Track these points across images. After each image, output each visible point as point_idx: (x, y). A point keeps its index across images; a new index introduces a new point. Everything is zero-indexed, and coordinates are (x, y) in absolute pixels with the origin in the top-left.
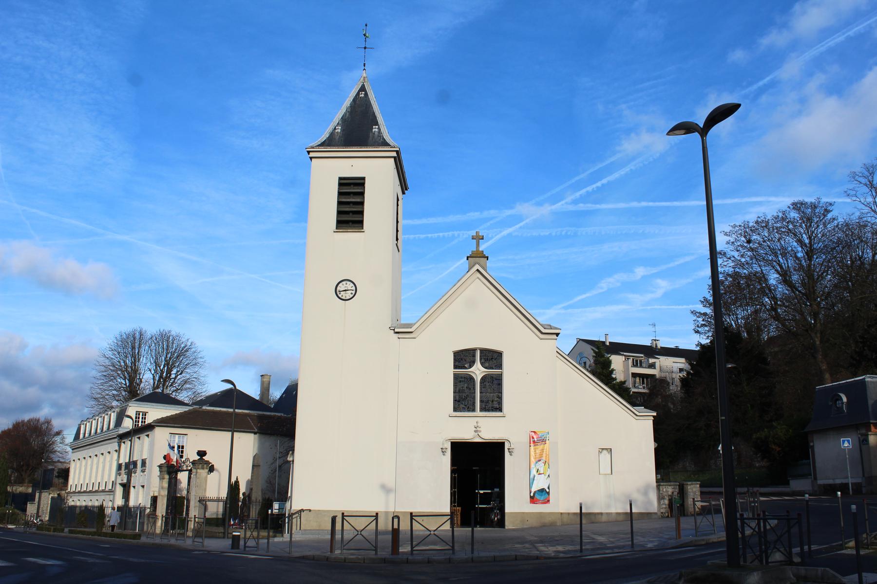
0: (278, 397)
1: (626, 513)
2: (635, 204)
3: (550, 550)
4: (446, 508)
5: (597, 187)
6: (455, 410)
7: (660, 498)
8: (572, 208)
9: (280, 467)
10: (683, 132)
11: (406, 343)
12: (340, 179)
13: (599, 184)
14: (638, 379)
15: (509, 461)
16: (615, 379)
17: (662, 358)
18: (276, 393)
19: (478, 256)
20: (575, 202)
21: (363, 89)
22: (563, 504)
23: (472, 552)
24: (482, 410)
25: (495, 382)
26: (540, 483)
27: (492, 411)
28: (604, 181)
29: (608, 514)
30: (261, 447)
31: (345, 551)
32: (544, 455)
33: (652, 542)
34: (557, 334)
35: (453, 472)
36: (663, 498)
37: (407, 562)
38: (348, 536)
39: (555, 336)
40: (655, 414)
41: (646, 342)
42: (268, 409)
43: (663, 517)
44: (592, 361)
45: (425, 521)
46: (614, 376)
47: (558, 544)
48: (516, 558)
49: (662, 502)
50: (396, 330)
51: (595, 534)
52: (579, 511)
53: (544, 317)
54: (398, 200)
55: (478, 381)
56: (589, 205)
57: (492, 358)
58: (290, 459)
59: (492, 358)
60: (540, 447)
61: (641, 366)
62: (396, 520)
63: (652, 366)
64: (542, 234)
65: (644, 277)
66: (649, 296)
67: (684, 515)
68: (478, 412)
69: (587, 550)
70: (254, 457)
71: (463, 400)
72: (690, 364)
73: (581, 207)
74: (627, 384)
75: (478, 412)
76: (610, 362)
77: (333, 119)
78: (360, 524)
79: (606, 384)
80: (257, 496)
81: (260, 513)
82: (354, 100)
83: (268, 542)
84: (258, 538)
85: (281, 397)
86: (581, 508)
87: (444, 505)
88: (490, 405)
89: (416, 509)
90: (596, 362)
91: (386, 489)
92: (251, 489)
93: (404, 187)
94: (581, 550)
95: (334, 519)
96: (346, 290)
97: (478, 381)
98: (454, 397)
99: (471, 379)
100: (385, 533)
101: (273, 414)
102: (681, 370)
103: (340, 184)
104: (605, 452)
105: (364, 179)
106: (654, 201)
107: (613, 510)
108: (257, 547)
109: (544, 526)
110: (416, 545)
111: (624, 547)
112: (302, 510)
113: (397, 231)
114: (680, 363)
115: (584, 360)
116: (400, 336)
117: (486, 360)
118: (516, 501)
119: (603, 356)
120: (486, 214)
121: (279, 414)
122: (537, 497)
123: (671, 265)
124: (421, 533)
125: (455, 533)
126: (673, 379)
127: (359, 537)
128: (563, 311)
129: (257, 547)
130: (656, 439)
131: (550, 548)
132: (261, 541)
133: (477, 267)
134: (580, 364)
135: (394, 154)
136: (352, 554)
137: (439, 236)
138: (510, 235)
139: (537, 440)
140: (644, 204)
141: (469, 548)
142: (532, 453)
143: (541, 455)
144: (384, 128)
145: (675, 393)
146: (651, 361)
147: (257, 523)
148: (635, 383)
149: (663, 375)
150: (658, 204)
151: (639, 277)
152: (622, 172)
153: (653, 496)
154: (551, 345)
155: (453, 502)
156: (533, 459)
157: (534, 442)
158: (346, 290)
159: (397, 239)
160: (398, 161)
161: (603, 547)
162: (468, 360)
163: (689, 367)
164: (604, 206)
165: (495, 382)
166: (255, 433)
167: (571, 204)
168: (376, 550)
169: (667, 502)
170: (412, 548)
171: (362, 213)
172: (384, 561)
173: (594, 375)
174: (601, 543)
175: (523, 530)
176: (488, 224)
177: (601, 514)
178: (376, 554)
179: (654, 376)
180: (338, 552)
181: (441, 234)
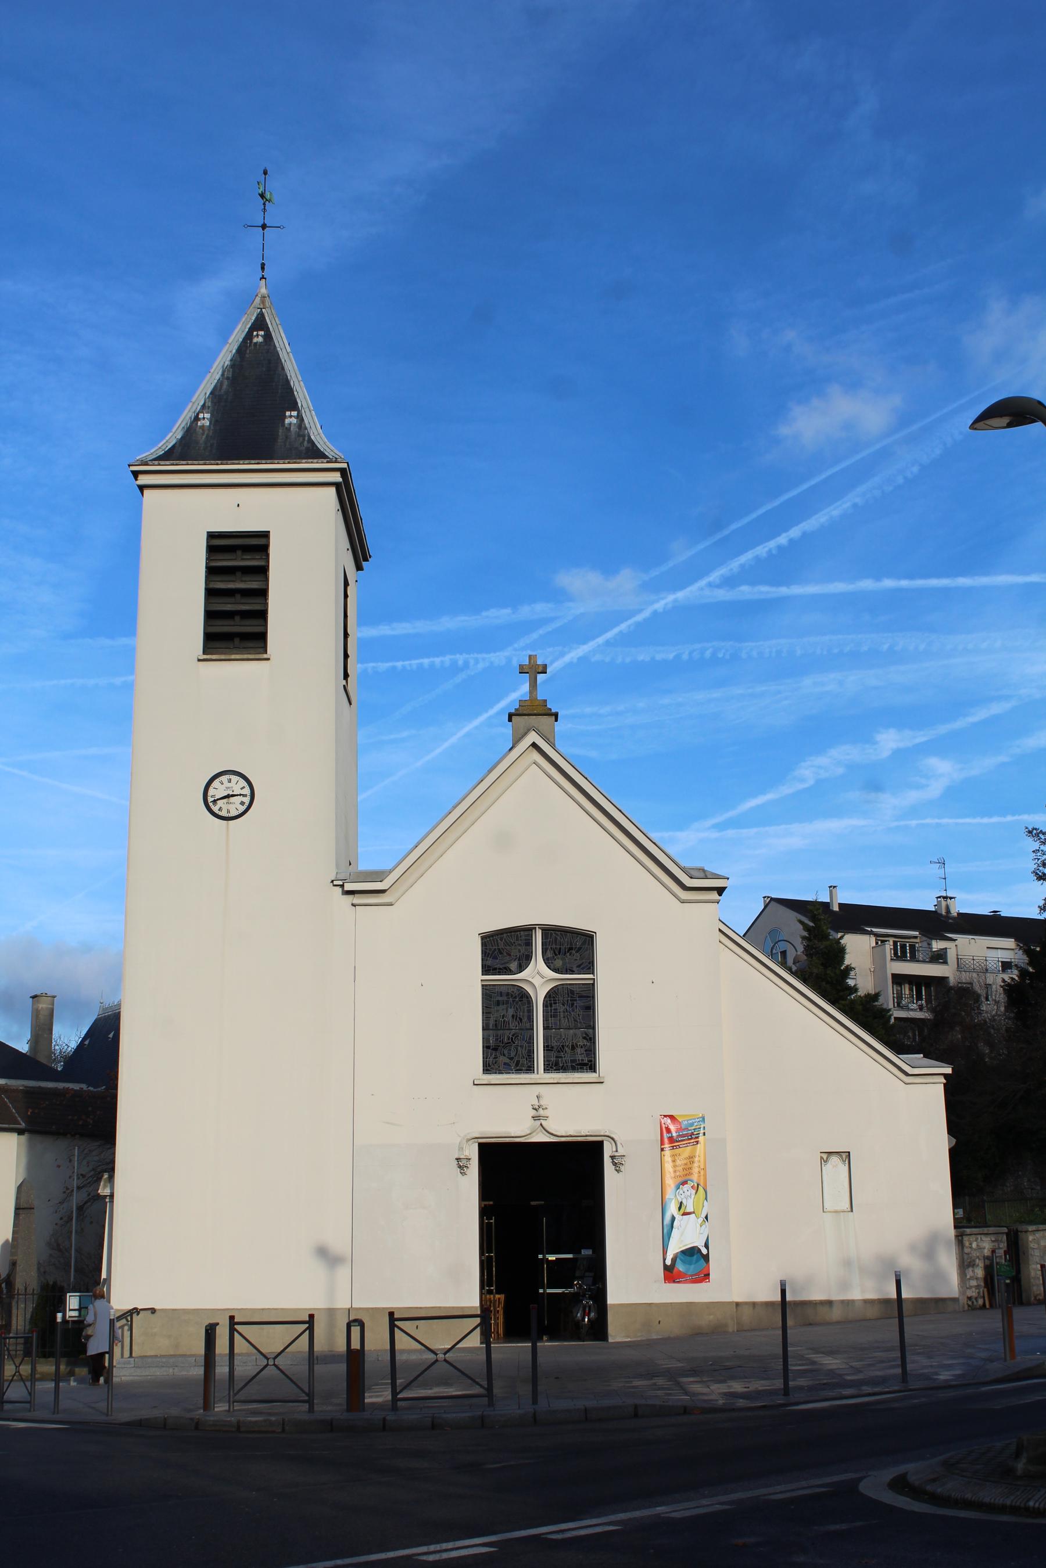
0: (73, 1045)
1: (885, 1302)
2: (867, 584)
3: (714, 1392)
4: (470, 1297)
5: (780, 548)
6: (487, 1069)
7: (965, 1264)
8: (723, 595)
9: (80, 1209)
10: (1006, 420)
11: (371, 916)
12: (211, 536)
13: (783, 540)
14: (906, 990)
15: (614, 1185)
16: (854, 989)
17: (962, 940)
18: (68, 1037)
19: (533, 712)
20: (729, 582)
21: (260, 323)
22: (741, 1280)
23: (535, 1401)
25: (579, 1003)
26: (687, 1235)
28: (795, 532)
29: (847, 1303)
30: (34, 1164)
31: (237, 1406)
32: (695, 1170)
33: (949, 1367)
34: (720, 891)
35: (484, 1212)
36: (972, 1264)
37: (385, 1426)
38: (245, 1368)
39: (714, 895)
40: (948, 1070)
41: (925, 901)
42: (47, 1073)
43: (972, 1308)
44: (801, 949)
45: (424, 1331)
46: (851, 982)
47: (733, 1378)
48: (636, 1412)
49: (969, 1273)
50: (348, 887)
51: (816, 1350)
52: (778, 1298)
53: (684, 845)
54: (346, 584)
55: (539, 1001)
56: (764, 589)
57: (572, 947)
58: (104, 1191)
59: (572, 947)
60: (686, 1151)
61: (914, 959)
62: (356, 1331)
63: (939, 957)
64: (659, 657)
65: (897, 753)
66: (913, 796)
67: (1021, 1303)
68: (540, 1074)
69: (801, 1388)
70: (19, 1189)
71: (505, 1048)
72: (1028, 952)
73: (745, 592)
74: (881, 1000)
75: (540, 1074)
76: (841, 951)
77: (192, 399)
78: (272, 1340)
79: (833, 1002)
80: (27, 1279)
81: (34, 1321)
82: (241, 351)
83: (57, 1387)
84: (33, 1378)
85: (81, 1046)
86: (783, 1292)
87: (469, 1295)
88: (567, 1057)
89: (403, 1300)
90: (809, 950)
91: (326, 1255)
92: (14, 1264)
93: (360, 553)
94: (786, 1391)
95: (210, 1332)
96: (228, 796)
97: (539, 1001)
98: (485, 1039)
99: (521, 998)
100: (331, 1358)
101: (61, 1085)
102: (1006, 966)
103: (211, 550)
104: (834, 1159)
105: (266, 535)
106: (911, 576)
107: (856, 1294)
108: (30, 1401)
109: (697, 1334)
110: (406, 1387)
111: (883, 1380)
112: (136, 1311)
113: (346, 656)
114: (1003, 949)
115: (782, 946)
116: (357, 899)
117: (557, 952)
118: (632, 1279)
119: (825, 937)
120: (526, 612)
121: (76, 1086)
122: (680, 1267)
123: (959, 724)
124: (413, 1357)
125: (494, 1356)
126: (988, 986)
127: (271, 1371)
128: (714, 835)
129: (30, 1401)
130: (953, 1128)
131: (714, 1387)
132: (40, 1386)
133: (533, 737)
134: (772, 956)
135: (337, 477)
136: (254, 1413)
138: (583, 660)
139: (678, 1135)
140: (888, 583)
141: (525, 1390)
142: (668, 1167)
143: (688, 1170)
144: (311, 415)
145: (993, 1019)
146: (937, 945)
147: (27, 1341)
148: (900, 997)
149: (965, 977)
150: (920, 583)
151: (886, 754)
152: (835, 511)
153: (948, 1262)
154: (704, 915)
155: (486, 1282)
156: (670, 1182)
157: (671, 1140)
158: (228, 796)
159: (346, 676)
160: (345, 492)
161: (836, 1382)
162: (515, 952)
163: (1025, 959)
164: (796, 590)
165: (579, 1003)
166: (20, 1132)
167: (718, 586)
168: (310, 1402)
169: (980, 1272)
170: (394, 1393)
172: (330, 1426)
173: (805, 981)
174: (831, 1373)
175: (649, 1344)
176: (535, 636)
177: (829, 1303)
178: (311, 1410)
179: (942, 980)
180: (220, 1407)
181: (426, 661)
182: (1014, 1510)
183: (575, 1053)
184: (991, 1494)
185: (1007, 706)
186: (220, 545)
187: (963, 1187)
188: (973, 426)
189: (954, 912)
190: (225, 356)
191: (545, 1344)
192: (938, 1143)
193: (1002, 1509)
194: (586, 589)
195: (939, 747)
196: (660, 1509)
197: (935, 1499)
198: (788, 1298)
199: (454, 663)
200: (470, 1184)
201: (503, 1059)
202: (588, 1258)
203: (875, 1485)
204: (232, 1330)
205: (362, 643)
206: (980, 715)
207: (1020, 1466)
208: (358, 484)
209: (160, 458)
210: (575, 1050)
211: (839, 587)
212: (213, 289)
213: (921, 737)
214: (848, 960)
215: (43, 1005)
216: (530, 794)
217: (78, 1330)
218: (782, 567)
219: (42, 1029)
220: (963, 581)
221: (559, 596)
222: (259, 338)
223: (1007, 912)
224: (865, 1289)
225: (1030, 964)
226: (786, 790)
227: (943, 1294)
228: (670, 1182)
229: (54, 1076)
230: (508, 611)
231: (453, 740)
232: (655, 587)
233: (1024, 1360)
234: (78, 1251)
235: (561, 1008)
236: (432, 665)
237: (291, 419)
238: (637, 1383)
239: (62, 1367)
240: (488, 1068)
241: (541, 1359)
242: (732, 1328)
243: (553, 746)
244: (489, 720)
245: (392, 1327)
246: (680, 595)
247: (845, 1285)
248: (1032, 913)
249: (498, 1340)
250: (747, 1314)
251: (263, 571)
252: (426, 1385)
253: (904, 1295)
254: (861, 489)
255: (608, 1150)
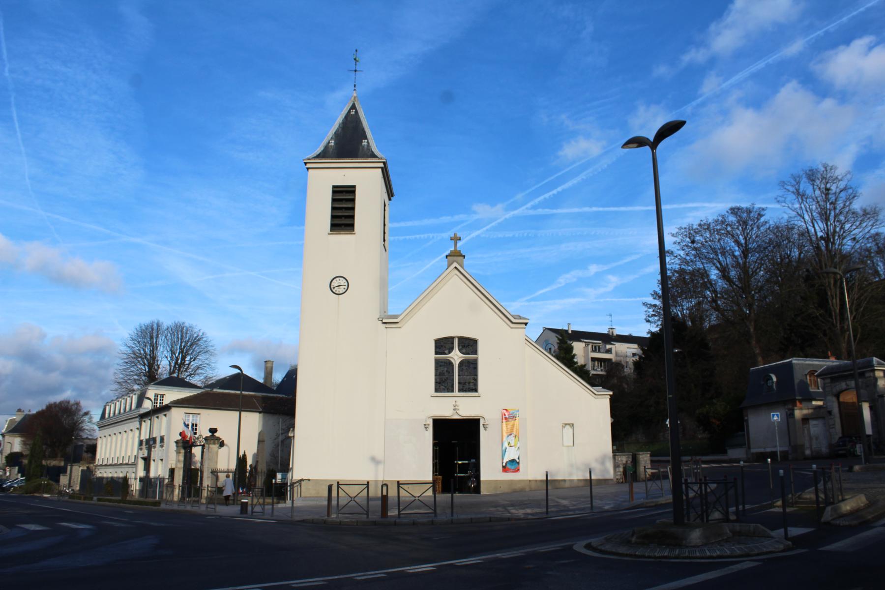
0: (280, 380)
1: (586, 480)
2: (587, 209)
3: (520, 513)
4: (430, 478)
7: (616, 466)
9: (282, 442)
11: (393, 332)
12: (334, 187)
13: (555, 192)
14: (596, 363)
16: (577, 363)
18: (278, 377)
19: (456, 255)
20: (534, 207)
21: (353, 107)
22: (532, 472)
23: (452, 515)
24: (460, 390)
25: (472, 366)
28: (560, 189)
30: (265, 424)
34: (526, 324)
35: (434, 445)
36: (618, 466)
37: (395, 524)
38: (342, 502)
39: (524, 326)
40: (611, 393)
42: (270, 390)
43: (618, 483)
45: (410, 488)
48: (490, 520)
51: (559, 498)
53: (513, 307)
55: (456, 364)
56: (547, 210)
57: (469, 345)
58: (291, 435)
59: (469, 345)
60: (511, 423)
61: (599, 352)
62: (385, 488)
63: (609, 351)
66: (602, 290)
68: (456, 392)
70: (260, 434)
72: (642, 349)
73: (540, 211)
74: (587, 367)
75: (456, 392)
77: (327, 134)
78: (353, 491)
79: (569, 367)
81: (265, 483)
82: (346, 117)
84: (264, 504)
85: (283, 380)
88: (467, 386)
89: (403, 478)
90: (560, 348)
91: (373, 459)
93: (390, 194)
94: (547, 512)
97: (456, 364)
99: (450, 364)
100: (375, 499)
102: (634, 355)
103: (334, 192)
104: (568, 427)
105: (354, 187)
107: (575, 478)
109: (515, 491)
111: (584, 509)
112: (302, 480)
115: (550, 346)
116: (388, 326)
117: (464, 347)
118: (490, 471)
119: (566, 343)
120: (457, 218)
122: (509, 466)
127: (353, 503)
128: (526, 304)
132: (266, 507)
133: (455, 265)
134: (546, 350)
135: (382, 165)
138: (478, 236)
139: (508, 417)
140: (595, 209)
141: (449, 511)
142: (505, 428)
143: (512, 430)
144: (372, 141)
146: (608, 347)
148: (594, 366)
149: (618, 359)
153: (610, 466)
154: (520, 333)
155: (435, 471)
156: (505, 434)
158: (338, 286)
161: (566, 509)
162: (447, 347)
164: (559, 211)
165: (472, 366)
166: (260, 412)
168: (367, 514)
169: (621, 469)
170: (399, 511)
172: (374, 523)
174: (564, 506)
175: (496, 495)
177: (565, 481)
179: (610, 360)
180: (334, 516)
181: (418, 236)
182: (631, 556)
183: (470, 385)
184: (622, 550)
185: (638, 256)
189: (615, 334)
190: (340, 119)
193: (627, 555)
194: (482, 211)
195: (612, 271)
196: (498, 555)
197: (601, 552)
200: (429, 435)
201: (442, 387)
203: (579, 546)
204: (338, 487)
207: (634, 539)
208: (389, 167)
209: (315, 158)
211: (576, 210)
212: (339, 95)
213: (606, 268)
214: (574, 352)
215: (269, 365)
216: (454, 286)
217: (284, 485)
218: (555, 202)
219: (269, 374)
220: (623, 209)
221: (475, 213)
222: (353, 113)
224: (579, 475)
226: (554, 287)
227: (608, 477)
228: (505, 434)
230: (449, 218)
231: (428, 266)
232: (507, 210)
233: (636, 502)
235: (465, 368)
237: (365, 143)
240: (436, 390)
241: (455, 500)
242: (527, 489)
244: (440, 259)
245: (399, 487)
246: (516, 212)
247: (571, 474)
250: (533, 485)
253: (593, 478)
254: (585, 173)
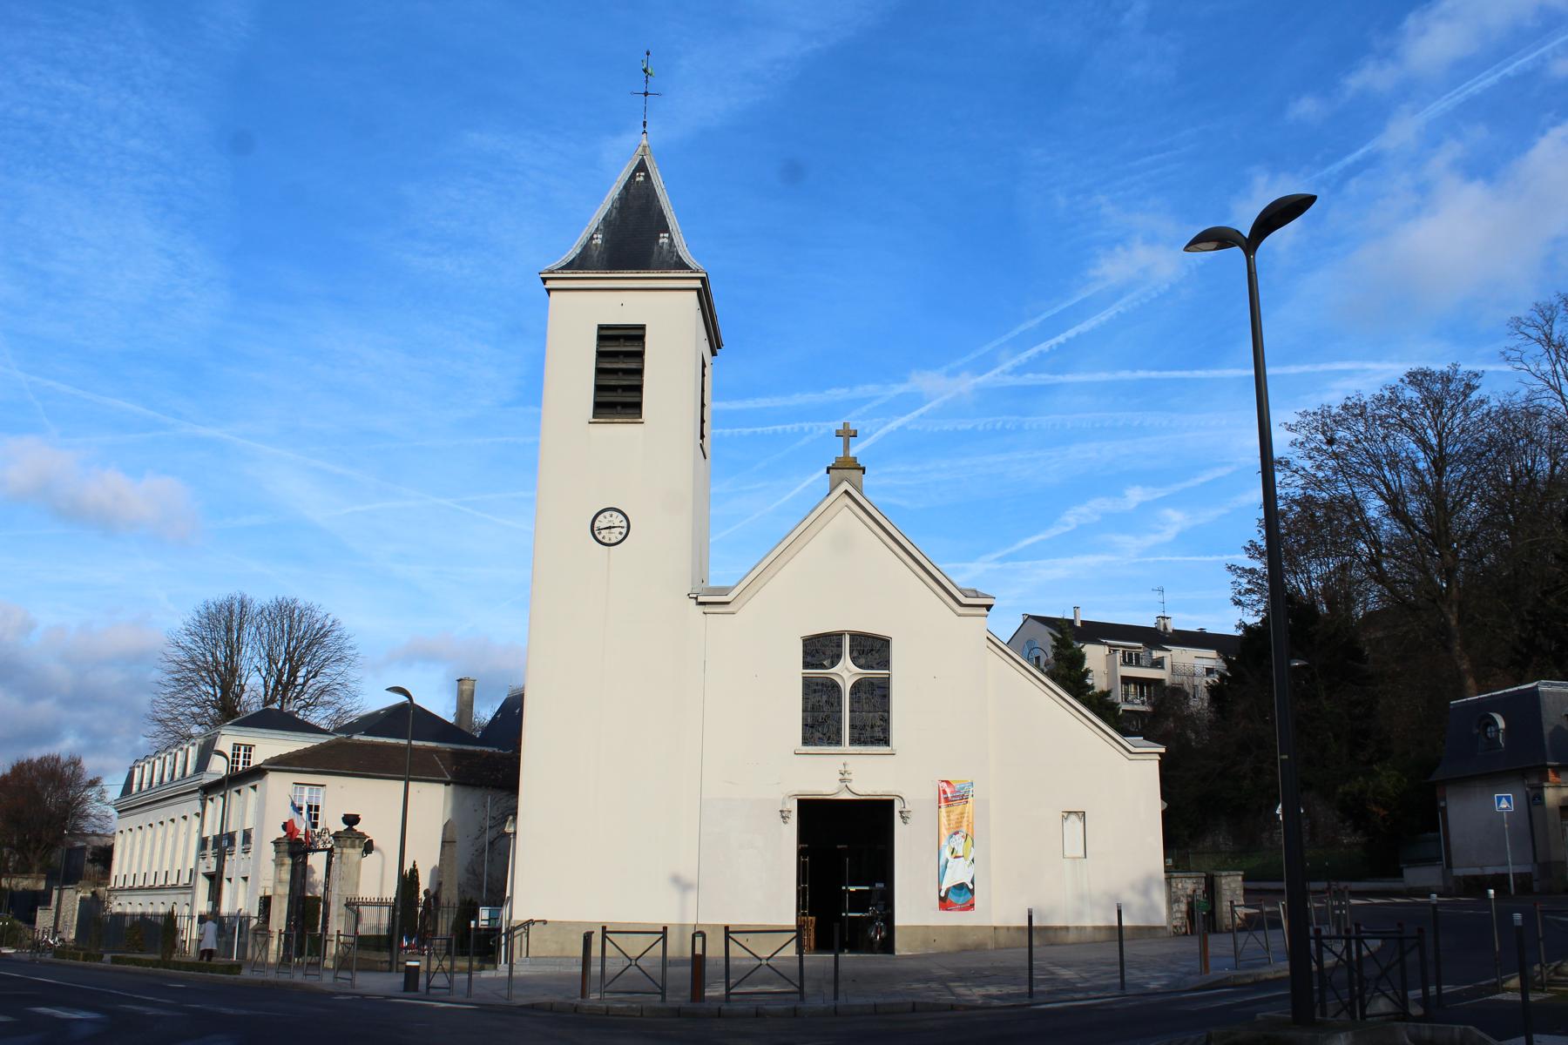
0: (489, 718)
1: (1111, 928)
2: (1125, 375)
5: (1059, 344)
6: (806, 742)
7: (1172, 900)
8: (1012, 381)
9: (491, 843)
10: (1214, 245)
11: (718, 622)
12: (601, 328)
13: (1061, 338)
14: (1132, 688)
16: (1092, 687)
18: (485, 712)
19: (846, 467)
20: (1019, 370)
21: (641, 167)
22: (999, 910)
23: (836, 998)
25: (877, 692)
27: (872, 743)
28: (1071, 333)
30: (457, 808)
31: (607, 996)
32: (965, 824)
33: (1157, 978)
34: (989, 607)
35: (800, 853)
36: (1178, 901)
37: (719, 1014)
38: (612, 968)
39: (984, 611)
40: (1163, 750)
43: (1176, 935)
44: (1051, 655)
45: (752, 942)
46: (1089, 682)
47: (990, 984)
48: (914, 1008)
49: (1175, 907)
50: (701, 599)
53: (964, 575)
54: (704, 366)
55: (846, 690)
57: (873, 649)
58: (509, 829)
59: (873, 649)
61: (1138, 664)
62: (699, 940)
63: (1158, 664)
66: (1152, 539)
67: (1215, 932)
68: (846, 747)
69: (1042, 993)
70: (445, 826)
71: (819, 725)
72: (1226, 661)
73: (1030, 378)
75: (846, 747)
76: (1082, 657)
78: (635, 946)
79: (1076, 696)
81: (454, 928)
83: (470, 979)
85: (494, 718)
87: (787, 915)
88: (868, 733)
89: (734, 921)
90: (1057, 657)
91: (681, 885)
92: (440, 884)
93: (715, 343)
95: (587, 938)
96: (611, 527)
97: (846, 690)
99: (833, 687)
100: (679, 962)
101: (478, 748)
102: (1209, 671)
103: (601, 338)
104: (1073, 817)
105: (643, 327)
106: (1159, 369)
107: (1088, 922)
108: (450, 987)
109: (964, 950)
111: (1106, 988)
112: (531, 922)
113: (703, 421)
114: (1208, 658)
115: (1037, 652)
116: (708, 609)
117: (861, 653)
118: (914, 907)
119: (1070, 646)
120: (860, 391)
122: (952, 897)
125: (805, 963)
126: (1195, 687)
128: (997, 566)
129: (450, 987)
132: (457, 977)
133: (845, 486)
134: (1028, 660)
135: (698, 284)
136: (620, 1001)
137: (775, 432)
138: (902, 428)
139: (952, 796)
140: (1141, 374)
141: (829, 990)
142: (944, 820)
143: (959, 823)
144: (680, 237)
146: (1156, 654)
147: (449, 944)
148: (1127, 694)
149: (1178, 680)
150: (1166, 374)
151: (1133, 506)
152: (1103, 317)
153: (1160, 897)
154: (976, 625)
155: (800, 907)
156: (945, 832)
157: (947, 799)
158: (611, 527)
159: (702, 436)
160: (704, 296)
162: (828, 652)
163: (1224, 666)
165: (877, 692)
166: (447, 783)
167: (1011, 374)
168: (663, 994)
169: (1183, 907)
170: (728, 989)
171: (639, 389)
172: (678, 1012)
173: (1053, 679)
174: (1066, 981)
175: (927, 957)
176: (864, 409)
177: (1067, 928)
179: (1160, 682)
180: (594, 996)
181: (779, 428)
186: (607, 335)
187: (1172, 842)
188: (1186, 249)
190: (614, 191)
191: (846, 956)
192: (1153, 806)
198: (1035, 924)
199: (802, 429)
201: (818, 735)
202: (880, 890)
204: (604, 937)
205: (714, 412)
206: (1207, 476)
210: (874, 730)
213: (1161, 493)
218: (1063, 359)
223: (1212, 629)
224: (1098, 918)
225: (1228, 669)
226: (1054, 532)
228: (945, 832)
229: (482, 741)
231: (798, 489)
233: (1214, 974)
234: (489, 875)
235: (864, 696)
236: (775, 432)
237: (663, 239)
238: (916, 986)
239: (475, 964)
242: (991, 945)
243: (861, 493)
245: (727, 938)
248: (1232, 631)
249: (809, 951)
251: (640, 355)
252: (751, 984)
253: (1124, 923)
254: (1124, 300)
255: (897, 807)
